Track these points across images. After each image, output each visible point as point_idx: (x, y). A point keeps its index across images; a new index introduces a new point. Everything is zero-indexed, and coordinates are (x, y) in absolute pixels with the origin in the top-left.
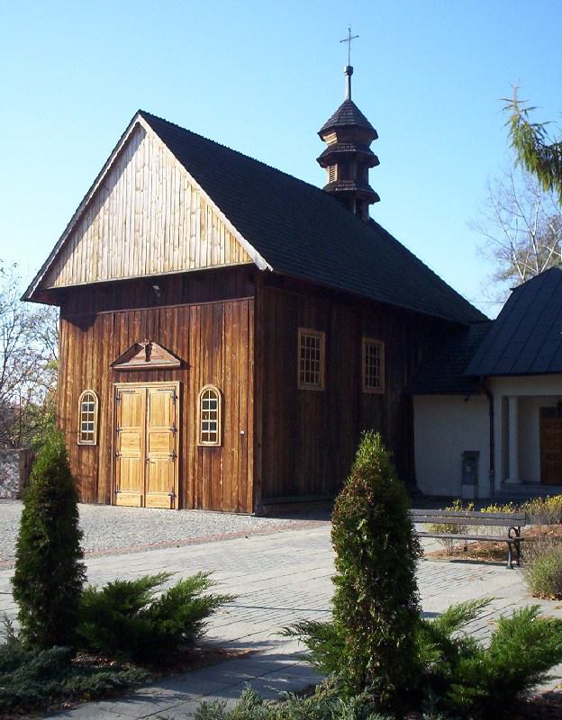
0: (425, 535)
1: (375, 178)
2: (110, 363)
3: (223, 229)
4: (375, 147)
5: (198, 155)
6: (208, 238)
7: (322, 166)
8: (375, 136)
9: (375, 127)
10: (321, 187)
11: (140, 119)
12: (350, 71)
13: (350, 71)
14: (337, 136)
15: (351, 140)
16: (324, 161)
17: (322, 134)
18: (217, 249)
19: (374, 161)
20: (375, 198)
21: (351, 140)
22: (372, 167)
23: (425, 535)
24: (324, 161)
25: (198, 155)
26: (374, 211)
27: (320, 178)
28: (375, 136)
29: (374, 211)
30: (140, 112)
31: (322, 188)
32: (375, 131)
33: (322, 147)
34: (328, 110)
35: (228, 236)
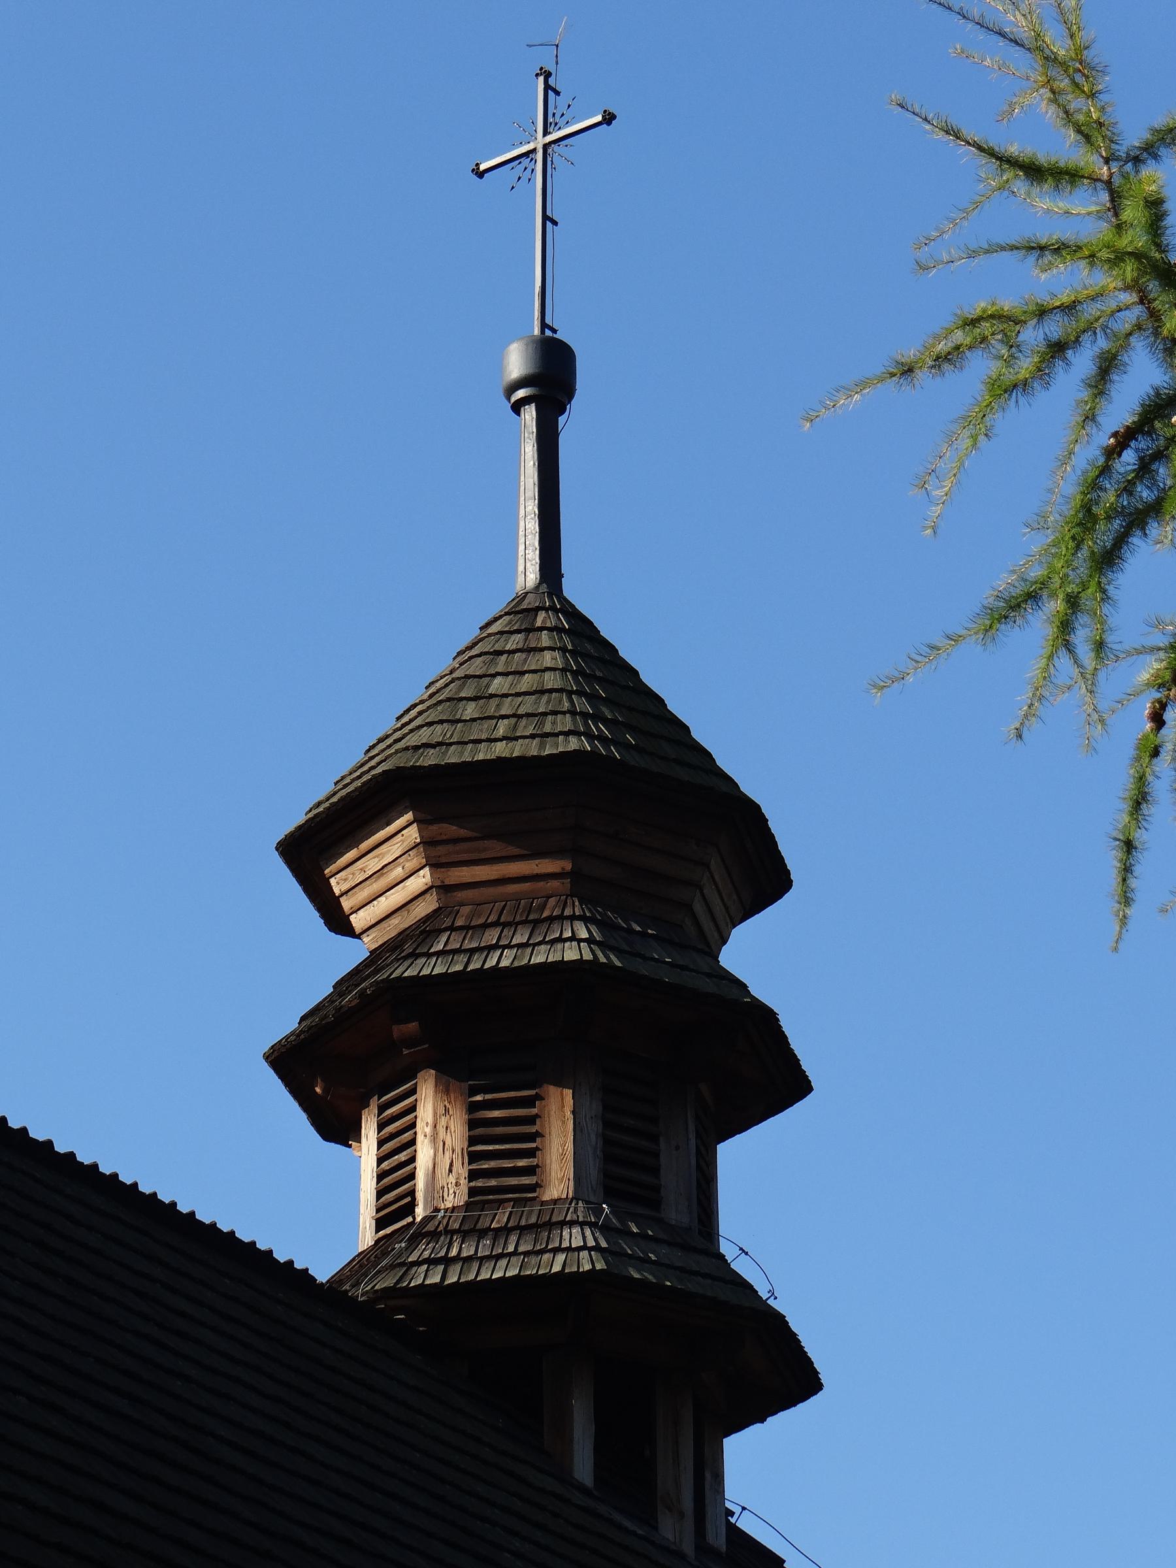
4: (775, 1210)
12: (552, 380)
13: (552, 380)
14: (434, 852)
16: (336, 1066)
17: (311, 851)
20: (771, 1369)
24: (336, 1066)
28: (763, 877)
32: (773, 1331)
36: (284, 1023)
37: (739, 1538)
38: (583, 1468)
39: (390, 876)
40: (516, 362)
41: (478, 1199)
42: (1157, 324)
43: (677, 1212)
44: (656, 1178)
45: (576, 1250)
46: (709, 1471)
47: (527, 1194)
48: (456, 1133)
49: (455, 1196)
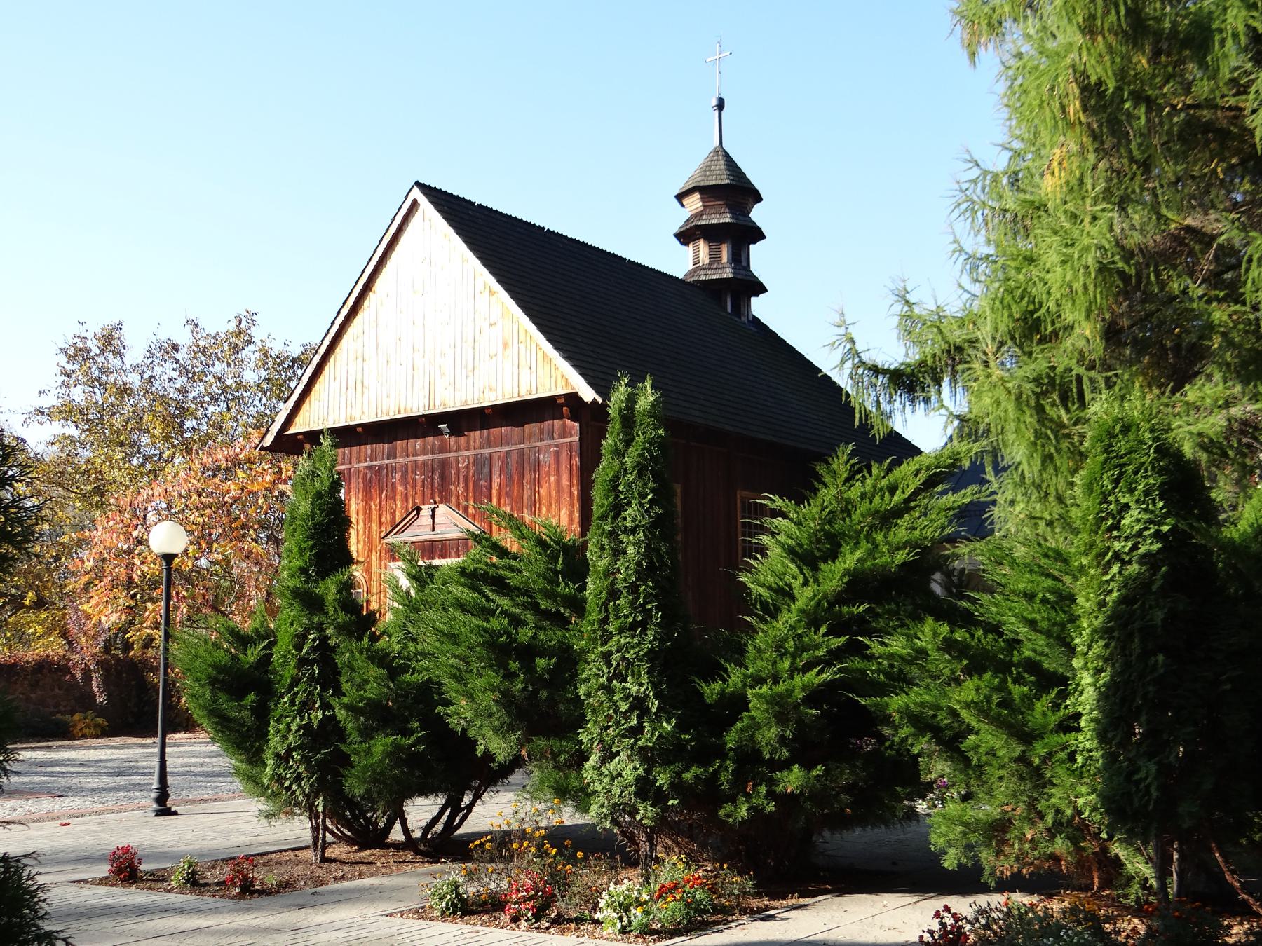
0: (696, 251)
1: (760, 259)
2: (383, 534)
3: (534, 346)
4: (758, 214)
5: (499, 240)
6: (516, 359)
7: (682, 244)
8: (758, 198)
9: (759, 224)
10: (680, 275)
11: (417, 194)
12: (721, 105)
13: (721, 105)
14: (702, 199)
15: (727, 211)
16: (686, 236)
17: (680, 197)
18: (525, 372)
19: (758, 235)
20: (760, 289)
21: (727, 211)
22: (757, 295)
23: (696, 251)
24: (686, 236)
25: (499, 240)
26: (759, 307)
27: (678, 262)
28: (758, 198)
29: (759, 307)
30: (417, 183)
31: (681, 276)
32: (759, 229)
33: (680, 216)
34: (689, 163)
35: (540, 354)
36: (676, 230)
37: (754, 317)
38: (729, 310)
39: (695, 202)
40: (715, 102)
41: (711, 263)
42: (1206, 264)
43: (744, 264)
44: (740, 259)
45: (728, 273)
46: (749, 301)
47: (719, 262)
48: (707, 250)
49: (707, 262)
